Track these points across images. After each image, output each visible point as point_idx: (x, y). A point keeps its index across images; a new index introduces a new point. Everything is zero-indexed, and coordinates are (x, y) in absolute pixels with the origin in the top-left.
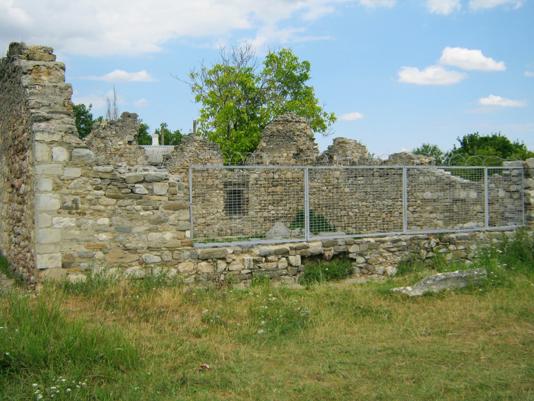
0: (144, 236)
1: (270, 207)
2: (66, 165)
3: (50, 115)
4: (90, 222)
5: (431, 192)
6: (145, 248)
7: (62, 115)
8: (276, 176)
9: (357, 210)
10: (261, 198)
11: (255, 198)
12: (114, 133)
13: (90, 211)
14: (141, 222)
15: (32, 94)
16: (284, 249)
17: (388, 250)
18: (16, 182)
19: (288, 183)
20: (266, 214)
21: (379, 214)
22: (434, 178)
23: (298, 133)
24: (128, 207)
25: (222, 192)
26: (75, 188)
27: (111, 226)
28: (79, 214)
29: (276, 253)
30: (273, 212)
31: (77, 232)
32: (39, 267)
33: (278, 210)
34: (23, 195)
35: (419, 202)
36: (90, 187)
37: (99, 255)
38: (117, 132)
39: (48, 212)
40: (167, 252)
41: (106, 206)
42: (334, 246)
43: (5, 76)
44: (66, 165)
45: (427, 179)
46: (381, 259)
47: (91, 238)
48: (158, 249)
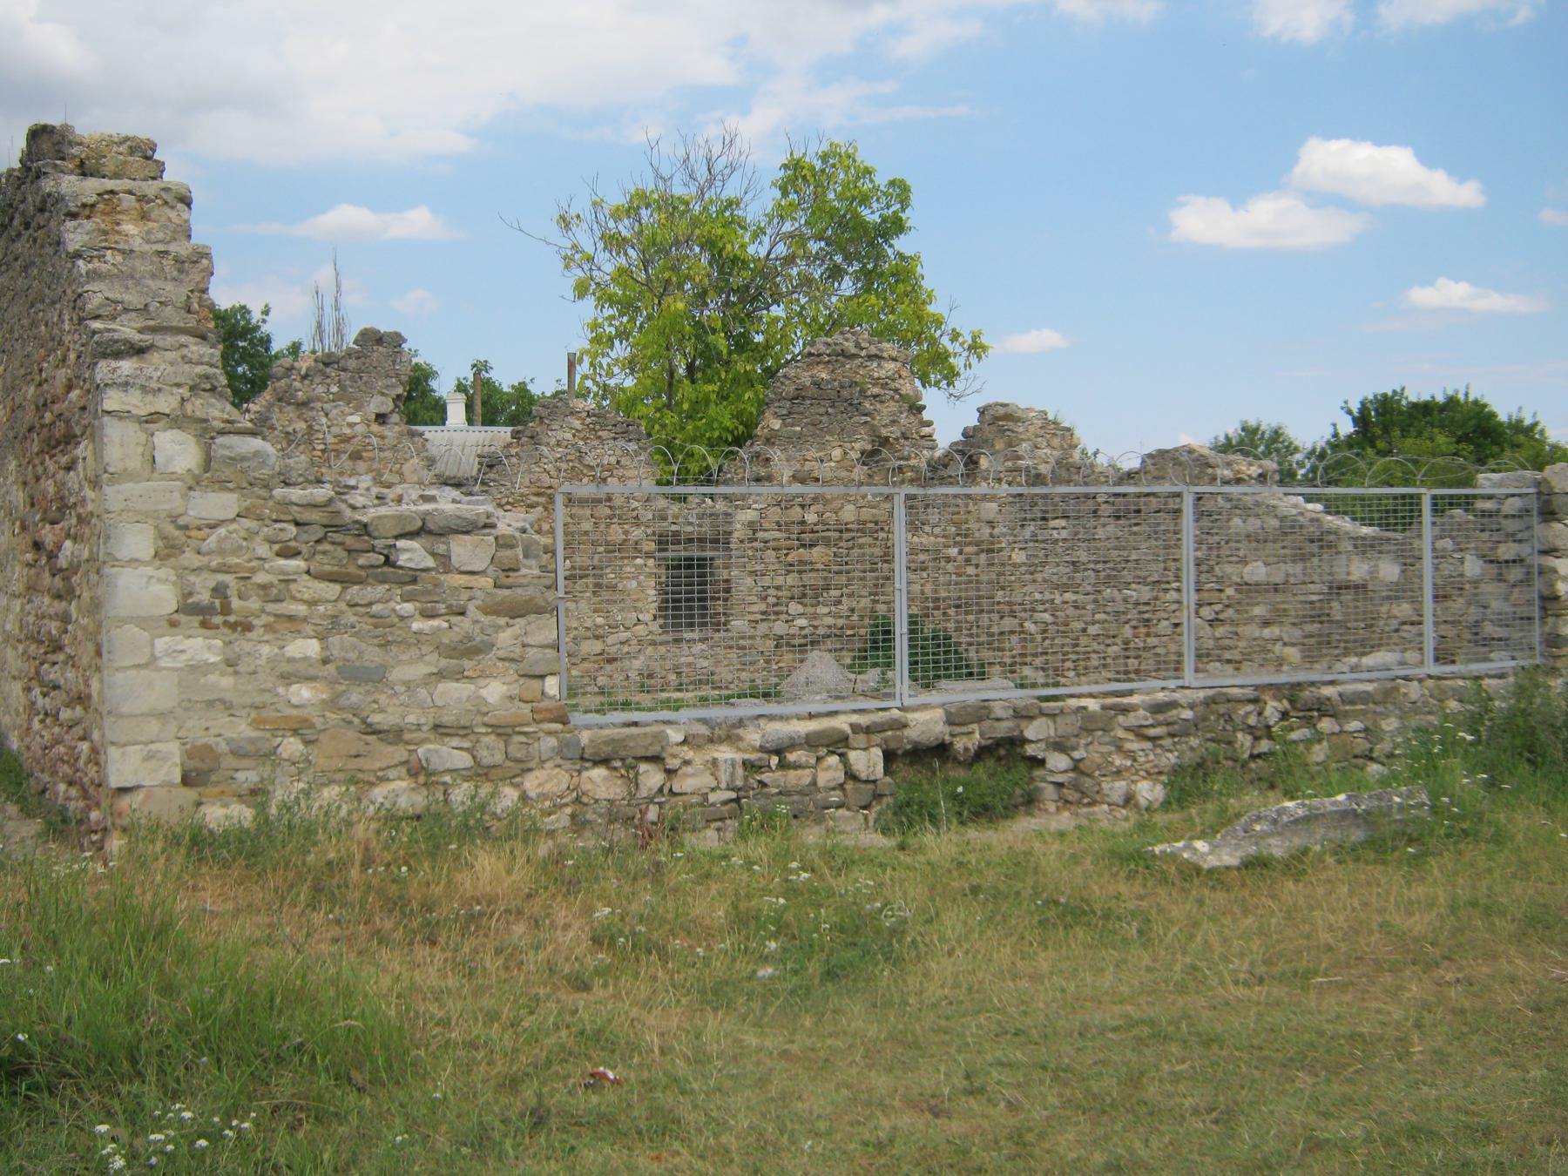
0: (423, 693)
1: (794, 608)
2: (194, 483)
3: (148, 338)
4: (266, 650)
5: (1266, 564)
6: (425, 728)
7: (183, 339)
8: (811, 518)
9: (1047, 617)
10: (767, 581)
11: (749, 581)
12: (335, 389)
13: (265, 619)
14: (414, 652)
15: (94, 275)
16: (834, 730)
17: (1139, 732)
18: (48, 535)
19: (846, 535)
20: (780, 628)
21: (1112, 628)
22: (1275, 523)
23: (876, 390)
24: (376, 608)
25: (651, 562)
26: (221, 552)
27: (325, 661)
28: (233, 627)
29: (811, 742)
30: (802, 622)
31: (227, 681)
32: (114, 782)
33: (815, 616)
34: (67, 573)
35: (1230, 591)
36: (263, 550)
37: (292, 746)
38: (342, 388)
39: (142, 622)
40: (490, 740)
41: (312, 603)
42: (979, 720)
43: (16, 223)
44: (194, 483)
45: (1254, 524)
46: (1118, 761)
47: (267, 698)
48: (464, 731)
